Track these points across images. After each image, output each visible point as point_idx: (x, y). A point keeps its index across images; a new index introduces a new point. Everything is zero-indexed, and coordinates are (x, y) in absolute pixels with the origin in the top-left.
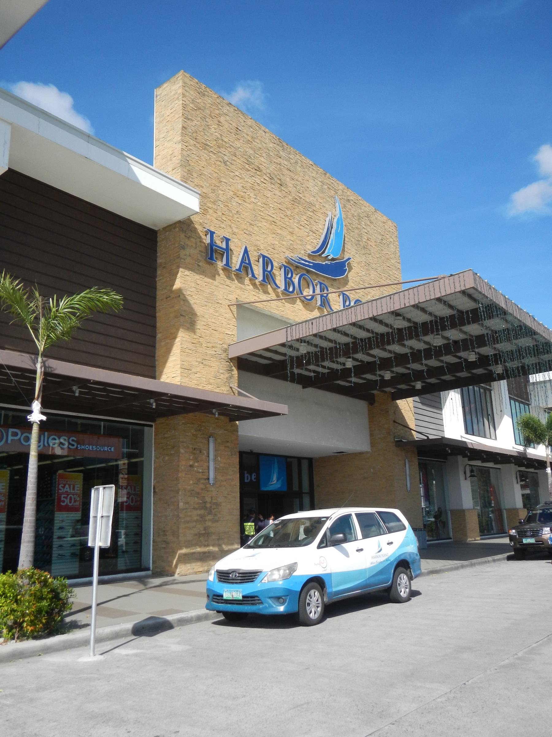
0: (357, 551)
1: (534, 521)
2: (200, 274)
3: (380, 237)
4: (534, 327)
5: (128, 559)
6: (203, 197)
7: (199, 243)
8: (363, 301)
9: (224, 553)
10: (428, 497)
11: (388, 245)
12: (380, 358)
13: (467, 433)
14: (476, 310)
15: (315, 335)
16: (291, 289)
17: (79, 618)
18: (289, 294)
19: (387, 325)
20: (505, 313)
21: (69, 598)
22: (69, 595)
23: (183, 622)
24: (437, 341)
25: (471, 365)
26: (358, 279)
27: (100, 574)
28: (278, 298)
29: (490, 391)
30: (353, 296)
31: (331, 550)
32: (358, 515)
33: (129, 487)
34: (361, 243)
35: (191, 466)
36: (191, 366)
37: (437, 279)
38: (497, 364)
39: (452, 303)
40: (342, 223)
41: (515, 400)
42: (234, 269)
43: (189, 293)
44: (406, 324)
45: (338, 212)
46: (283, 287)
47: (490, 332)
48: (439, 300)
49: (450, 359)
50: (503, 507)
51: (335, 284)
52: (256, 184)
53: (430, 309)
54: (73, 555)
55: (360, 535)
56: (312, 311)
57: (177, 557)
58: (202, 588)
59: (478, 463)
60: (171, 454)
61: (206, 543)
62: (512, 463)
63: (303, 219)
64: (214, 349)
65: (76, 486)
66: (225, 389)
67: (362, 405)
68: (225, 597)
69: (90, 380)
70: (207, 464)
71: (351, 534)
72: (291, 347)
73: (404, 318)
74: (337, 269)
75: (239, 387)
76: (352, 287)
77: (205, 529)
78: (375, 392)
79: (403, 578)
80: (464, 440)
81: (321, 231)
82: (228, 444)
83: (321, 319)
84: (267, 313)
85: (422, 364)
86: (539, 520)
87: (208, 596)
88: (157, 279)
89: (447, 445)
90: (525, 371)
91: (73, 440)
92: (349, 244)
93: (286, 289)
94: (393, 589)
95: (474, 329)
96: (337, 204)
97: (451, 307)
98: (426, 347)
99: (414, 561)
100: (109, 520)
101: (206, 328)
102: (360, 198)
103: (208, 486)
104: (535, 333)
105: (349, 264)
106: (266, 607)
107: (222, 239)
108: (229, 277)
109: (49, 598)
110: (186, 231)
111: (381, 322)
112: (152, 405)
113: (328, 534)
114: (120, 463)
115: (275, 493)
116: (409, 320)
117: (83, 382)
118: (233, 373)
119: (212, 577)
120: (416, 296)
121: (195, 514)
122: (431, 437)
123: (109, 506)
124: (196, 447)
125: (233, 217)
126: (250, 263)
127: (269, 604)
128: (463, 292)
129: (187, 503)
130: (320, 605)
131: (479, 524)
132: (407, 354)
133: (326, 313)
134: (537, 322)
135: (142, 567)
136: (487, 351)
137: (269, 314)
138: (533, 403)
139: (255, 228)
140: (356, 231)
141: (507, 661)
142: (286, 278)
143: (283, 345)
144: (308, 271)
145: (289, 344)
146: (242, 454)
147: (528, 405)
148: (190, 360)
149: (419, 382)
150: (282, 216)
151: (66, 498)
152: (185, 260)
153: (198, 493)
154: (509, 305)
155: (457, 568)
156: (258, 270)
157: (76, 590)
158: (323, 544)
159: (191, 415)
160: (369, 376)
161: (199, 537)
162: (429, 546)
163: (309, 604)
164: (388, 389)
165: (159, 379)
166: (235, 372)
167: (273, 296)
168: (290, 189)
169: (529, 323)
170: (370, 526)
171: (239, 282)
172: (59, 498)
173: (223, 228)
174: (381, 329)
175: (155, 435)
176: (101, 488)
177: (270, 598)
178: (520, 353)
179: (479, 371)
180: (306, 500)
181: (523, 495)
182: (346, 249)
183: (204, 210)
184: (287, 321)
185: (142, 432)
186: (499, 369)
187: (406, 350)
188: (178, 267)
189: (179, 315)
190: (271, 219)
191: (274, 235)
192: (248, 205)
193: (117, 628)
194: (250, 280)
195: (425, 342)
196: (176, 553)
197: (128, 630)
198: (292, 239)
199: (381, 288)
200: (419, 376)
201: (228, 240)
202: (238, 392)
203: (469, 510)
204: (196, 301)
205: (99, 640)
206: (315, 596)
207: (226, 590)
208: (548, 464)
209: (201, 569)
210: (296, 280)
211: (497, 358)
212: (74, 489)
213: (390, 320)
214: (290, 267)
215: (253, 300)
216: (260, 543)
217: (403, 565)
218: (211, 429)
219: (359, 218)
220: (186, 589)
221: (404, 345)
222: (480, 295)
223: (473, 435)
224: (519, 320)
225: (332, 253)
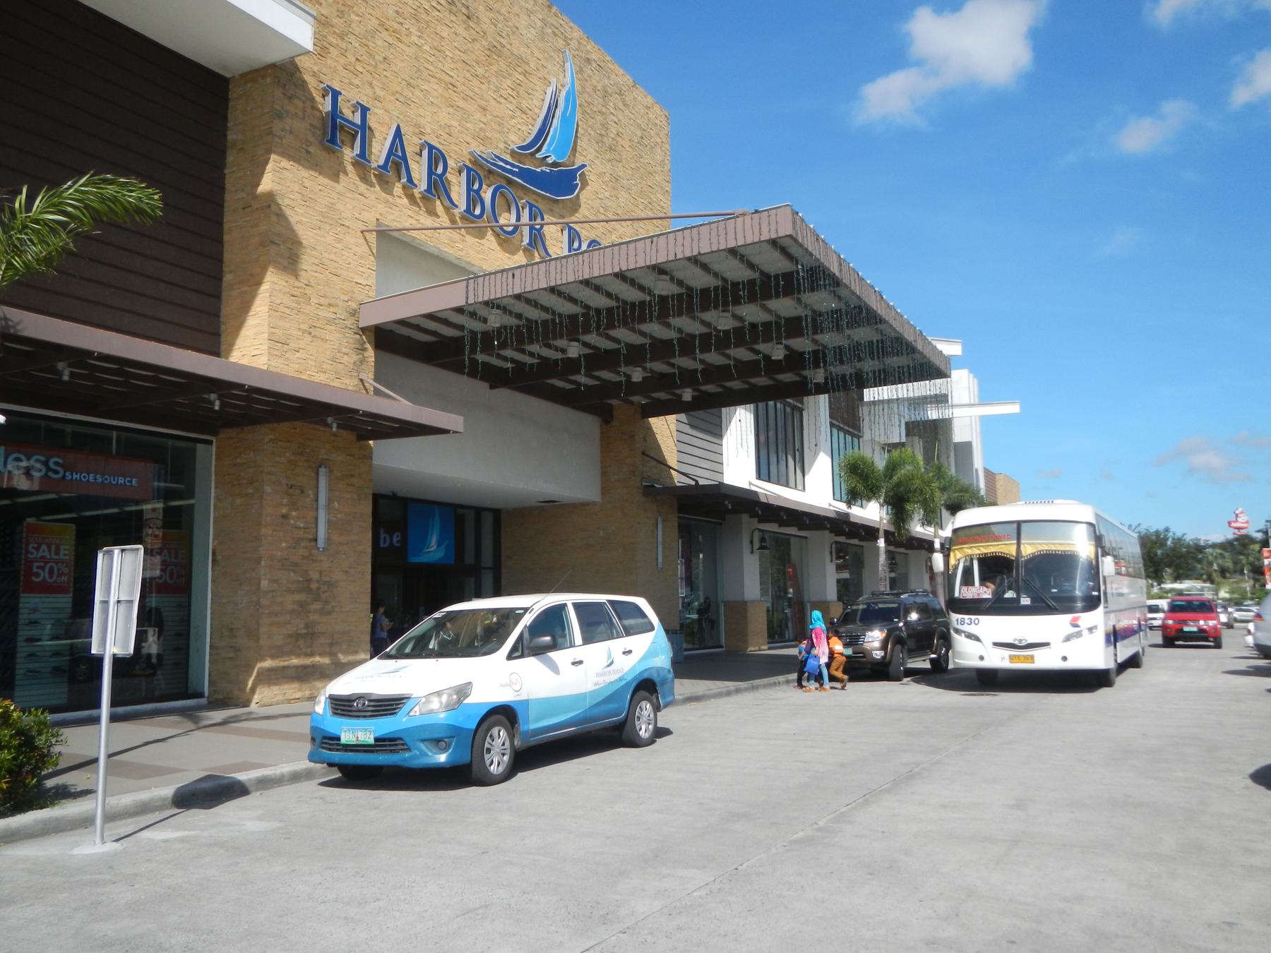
0: (573, 663)
1: (853, 622)
2: (310, 168)
3: (639, 133)
4: (881, 311)
5: (165, 678)
6: (321, 23)
7: (309, 110)
8: (604, 243)
9: (340, 669)
10: (689, 581)
11: (652, 148)
12: (627, 345)
13: (759, 477)
14: (791, 274)
15: (518, 297)
16: (477, 212)
17: (73, 780)
18: (473, 219)
19: (642, 288)
20: (837, 282)
21: (51, 745)
22: (53, 741)
23: (265, 783)
24: (723, 321)
25: (772, 366)
26: (596, 203)
27: (114, 703)
28: (454, 225)
29: (801, 410)
30: (586, 233)
31: (531, 663)
32: (577, 606)
33: (165, 552)
34: (605, 140)
35: (284, 517)
36: (286, 337)
37: (732, 216)
38: (817, 366)
39: (752, 259)
40: (574, 102)
41: (839, 429)
42: (374, 165)
43: (287, 202)
44: (674, 289)
45: (568, 79)
46: (463, 207)
47: (810, 313)
48: (733, 252)
49: (742, 354)
50: (806, 599)
51: (556, 209)
52: (421, 10)
53: (716, 267)
54: (57, 670)
55: (578, 637)
56: (513, 253)
57: (255, 674)
58: (304, 726)
59: (772, 527)
60: (247, 495)
61: (309, 651)
62: (826, 529)
63: (504, 86)
64: (332, 309)
65: (62, 547)
66: (350, 383)
67: (589, 424)
68: (344, 740)
69: (93, 352)
70: (312, 514)
71: (564, 636)
72: (473, 315)
73: (672, 279)
74: (562, 183)
75: (376, 380)
76: (585, 216)
77: (307, 626)
78: (614, 402)
79: (646, 708)
80: (754, 488)
81: (537, 111)
82: (353, 480)
83: (529, 269)
84: (431, 250)
85: (695, 359)
86: (861, 620)
87: (313, 739)
88: (226, 171)
89: (727, 497)
90: (862, 382)
91: (56, 463)
92: (585, 139)
93: (468, 210)
94: (628, 724)
95: (784, 306)
96: (568, 65)
97: (751, 266)
98: (704, 330)
99: (664, 682)
100: (131, 608)
101: (318, 269)
102: (608, 58)
103: (314, 551)
104: (882, 321)
105: (583, 175)
106: (415, 757)
107: (354, 106)
108: (364, 179)
109: (15, 747)
110: (285, 86)
111: (633, 282)
112: (212, 403)
113: (526, 635)
114: (147, 507)
115: (431, 569)
116: (680, 283)
117: (78, 356)
118: (366, 354)
119: (321, 707)
120: (695, 242)
121: (290, 601)
122: (702, 482)
123: (133, 583)
124: (294, 482)
125: (376, 67)
126: (404, 158)
127: (421, 751)
128: (774, 243)
129: (276, 581)
130: (508, 752)
131: (768, 629)
132: (672, 340)
133: (537, 259)
134: (885, 302)
135: (190, 691)
136: (803, 344)
137: (436, 253)
138: (867, 435)
139: (417, 93)
140: (599, 118)
141: (801, 834)
142: (469, 189)
143: (459, 310)
144: (510, 182)
145: (471, 309)
146: (377, 498)
147: (859, 437)
148: (287, 325)
149: (689, 390)
150: (468, 75)
151: (43, 568)
152: (281, 138)
153: (296, 564)
154: (845, 270)
155: (729, 694)
156: (419, 170)
157: (67, 732)
158: (517, 652)
159: (285, 426)
160: (606, 375)
161: (297, 640)
162: (687, 657)
163: (489, 751)
164: (636, 399)
165: (227, 358)
166: (370, 353)
167: (444, 220)
168: (485, 27)
169: (873, 303)
170: (597, 625)
171: (384, 190)
172: (30, 568)
173: (357, 87)
174: (632, 295)
175: (218, 459)
176: (116, 551)
177: (423, 741)
178: (857, 351)
179: (787, 377)
180: (488, 580)
181: (838, 581)
182: (579, 149)
183: (322, 48)
184: (467, 267)
185: (193, 452)
186: (819, 376)
187: (672, 335)
188: (269, 152)
189: (268, 241)
190: (447, 79)
191: (451, 110)
192: (405, 48)
193: (144, 796)
194: (404, 188)
195: (704, 323)
196: (253, 668)
197: (165, 799)
198: (484, 120)
199: (636, 224)
200: (688, 378)
201: (365, 110)
202: (375, 389)
203: (753, 601)
204: (300, 218)
205: (111, 817)
206: (500, 738)
207: (345, 728)
208: (881, 533)
209: (298, 695)
210: (487, 195)
211: (818, 358)
212: (57, 553)
213: (648, 280)
214: (477, 171)
215: (407, 225)
216: (408, 650)
217: (646, 687)
218: (323, 451)
219: (606, 95)
220: (272, 729)
221: (668, 325)
222: (800, 250)
223: (769, 480)
224: (859, 297)
225: (555, 152)
